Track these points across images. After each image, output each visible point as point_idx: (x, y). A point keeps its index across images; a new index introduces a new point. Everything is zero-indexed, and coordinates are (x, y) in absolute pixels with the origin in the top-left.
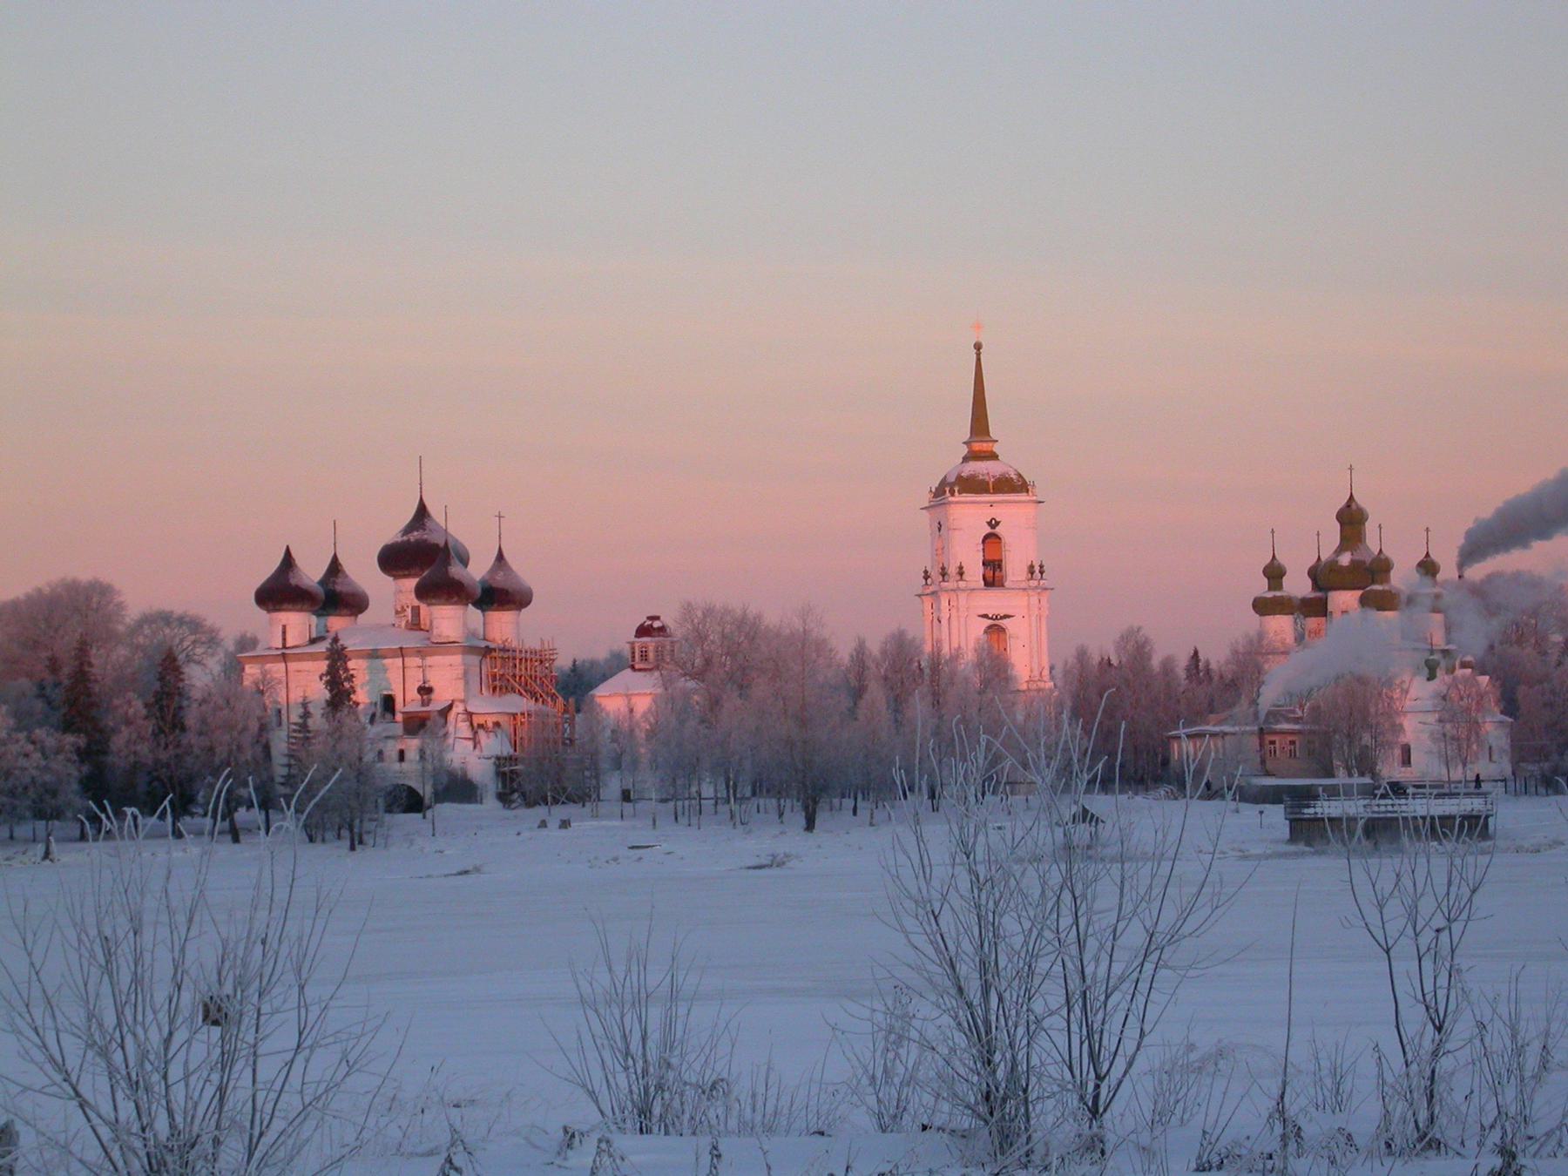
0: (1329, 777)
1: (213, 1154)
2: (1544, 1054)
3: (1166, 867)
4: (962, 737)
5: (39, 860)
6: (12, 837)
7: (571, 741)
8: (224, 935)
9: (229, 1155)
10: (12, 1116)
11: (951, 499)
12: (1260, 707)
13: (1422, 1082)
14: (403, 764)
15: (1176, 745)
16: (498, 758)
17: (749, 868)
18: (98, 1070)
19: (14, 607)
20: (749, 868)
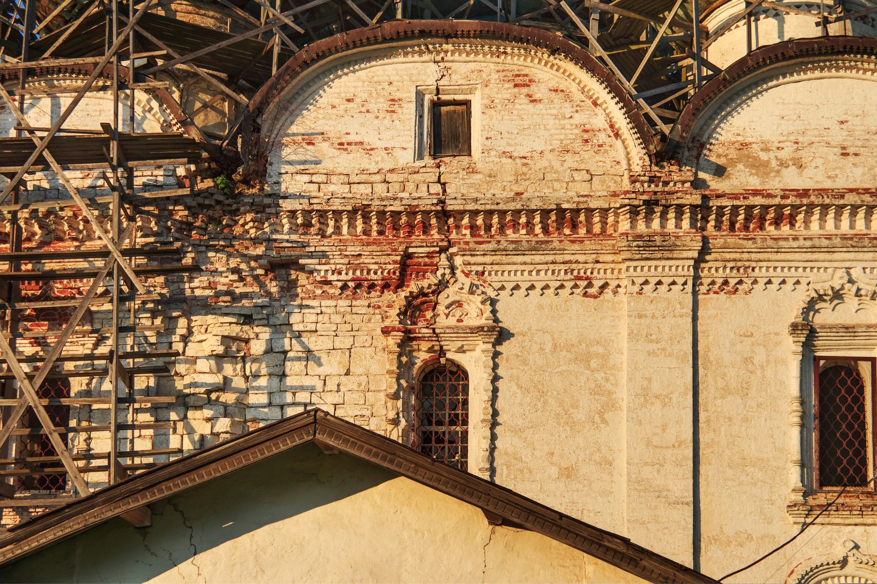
0: (370, 17)
1: (805, 239)
2: (737, 145)
3: (129, 363)
4: (58, 520)
5: (343, 95)
6: (860, 578)
7: (490, 176)
8: (641, 202)
9: (226, 302)
10: (532, 283)
11: (531, 65)
12: (788, 158)
13: (203, 390)
14: (452, 165)
15: (179, 313)
16: (223, 336)
17: (205, 340)
18: (395, 188)
19: (2, 565)
20: (205, 340)
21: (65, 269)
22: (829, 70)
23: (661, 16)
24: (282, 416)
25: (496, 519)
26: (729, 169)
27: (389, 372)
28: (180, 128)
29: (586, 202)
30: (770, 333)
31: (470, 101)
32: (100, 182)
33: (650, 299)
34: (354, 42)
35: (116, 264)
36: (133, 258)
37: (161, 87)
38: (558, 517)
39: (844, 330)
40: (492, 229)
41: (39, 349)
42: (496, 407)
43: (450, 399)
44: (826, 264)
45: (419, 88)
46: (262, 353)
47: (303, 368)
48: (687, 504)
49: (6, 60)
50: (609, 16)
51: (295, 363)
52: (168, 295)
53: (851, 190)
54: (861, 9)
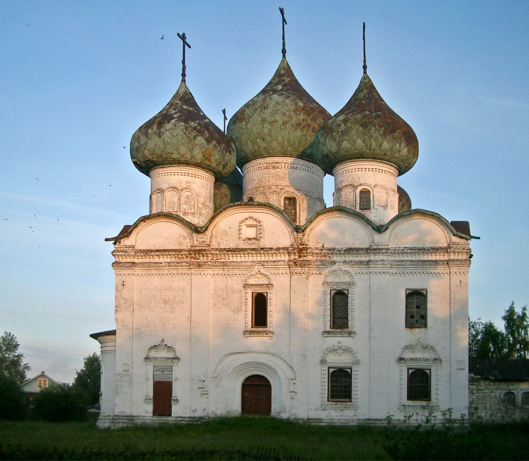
21: (333, 423)
22: (155, 221)
23: (502, 355)
24: (150, 211)
25: (182, 61)
26: (158, 138)
27: (494, 323)
28: (177, 121)
29: (233, 151)
30: (291, 402)
31: (406, 327)
32: (181, 128)
33: (123, 324)
34: (357, 398)
35: (331, 153)
36: (20, 386)
37: (360, 94)
38: (400, 205)
39: (316, 267)
40: (300, 126)
41: (16, 354)
42: (263, 352)
43: (342, 395)
44: (162, 172)
45: (349, 400)
46: (150, 179)
47: (169, 132)
48: (150, 399)
49: (174, 362)
50: (497, 339)
51: (426, 260)
52: (190, 122)
53: (265, 284)
54: (429, 212)
